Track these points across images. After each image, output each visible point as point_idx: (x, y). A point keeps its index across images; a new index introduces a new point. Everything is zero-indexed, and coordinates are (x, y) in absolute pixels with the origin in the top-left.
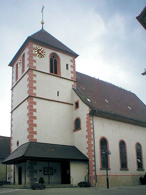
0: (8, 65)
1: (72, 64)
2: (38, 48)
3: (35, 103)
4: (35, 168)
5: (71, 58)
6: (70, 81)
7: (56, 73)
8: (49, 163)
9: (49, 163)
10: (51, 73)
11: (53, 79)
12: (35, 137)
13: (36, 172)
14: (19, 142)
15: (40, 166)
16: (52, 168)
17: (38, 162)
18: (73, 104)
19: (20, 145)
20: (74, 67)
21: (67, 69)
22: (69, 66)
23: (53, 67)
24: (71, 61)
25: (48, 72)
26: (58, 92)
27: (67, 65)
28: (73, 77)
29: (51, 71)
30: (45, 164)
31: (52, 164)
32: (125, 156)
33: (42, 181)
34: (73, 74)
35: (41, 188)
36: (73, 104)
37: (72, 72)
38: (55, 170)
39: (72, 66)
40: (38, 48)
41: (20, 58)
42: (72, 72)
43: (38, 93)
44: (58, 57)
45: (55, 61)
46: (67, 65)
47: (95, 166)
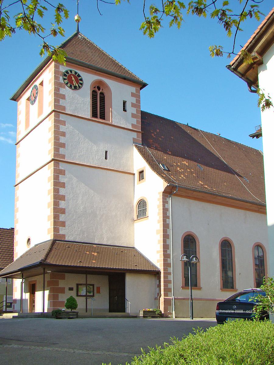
0: (11, 97)
1: (134, 100)
2: (70, 73)
3: (64, 123)
4: (62, 284)
5: (133, 89)
6: (129, 132)
7: (103, 117)
8: (86, 276)
9: (86, 276)
10: (94, 119)
11: (97, 127)
12: (62, 231)
13: (62, 291)
14: (31, 241)
15: (71, 281)
16: (93, 285)
17: (66, 274)
18: (134, 174)
19: (32, 245)
20: (137, 105)
21: (125, 110)
22: (128, 106)
23: (97, 98)
24: (133, 95)
25: (88, 114)
26: (106, 152)
27: (124, 103)
28: (136, 124)
29: (94, 115)
30: (81, 279)
31: (92, 280)
32: (238, 303)
33: (71, 304)
34: (135, 120)
35: (71, 317)
36: (134, 173)
37: (133, 116)
38: (98, 289)
39: (133, 105)
40: (70, 73)
41: (32, 126)
42: (133, 116)
43: (70, 155)
44: (106, 86)
45: (102, 95)
46: (124, 103)
47: (163, 209)
